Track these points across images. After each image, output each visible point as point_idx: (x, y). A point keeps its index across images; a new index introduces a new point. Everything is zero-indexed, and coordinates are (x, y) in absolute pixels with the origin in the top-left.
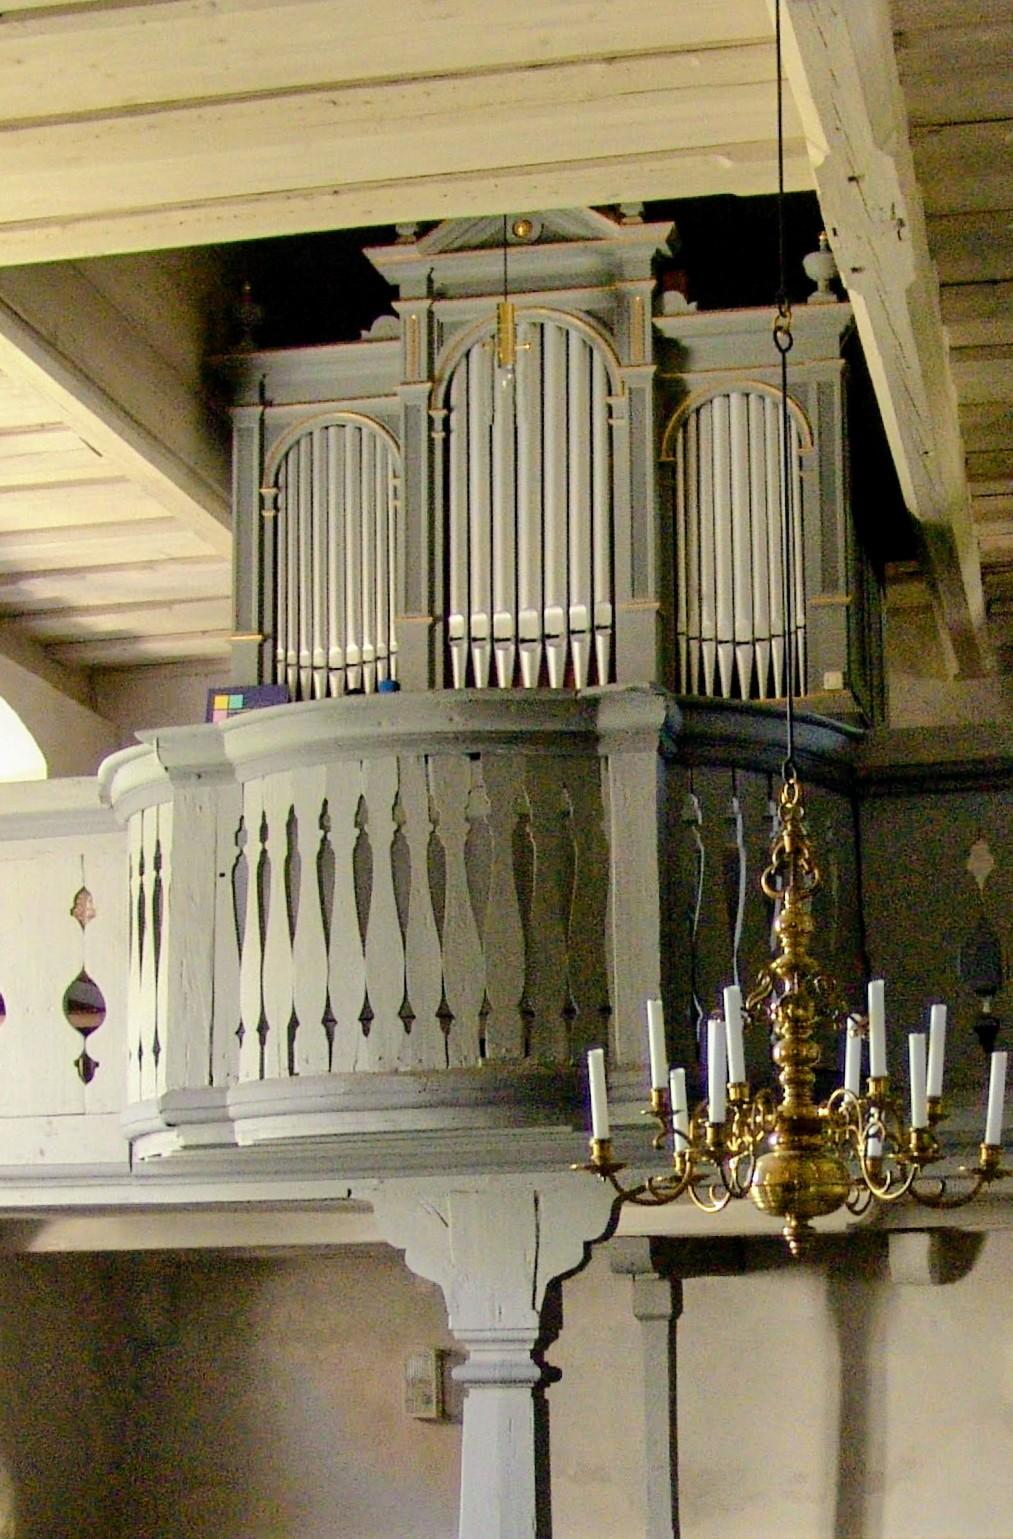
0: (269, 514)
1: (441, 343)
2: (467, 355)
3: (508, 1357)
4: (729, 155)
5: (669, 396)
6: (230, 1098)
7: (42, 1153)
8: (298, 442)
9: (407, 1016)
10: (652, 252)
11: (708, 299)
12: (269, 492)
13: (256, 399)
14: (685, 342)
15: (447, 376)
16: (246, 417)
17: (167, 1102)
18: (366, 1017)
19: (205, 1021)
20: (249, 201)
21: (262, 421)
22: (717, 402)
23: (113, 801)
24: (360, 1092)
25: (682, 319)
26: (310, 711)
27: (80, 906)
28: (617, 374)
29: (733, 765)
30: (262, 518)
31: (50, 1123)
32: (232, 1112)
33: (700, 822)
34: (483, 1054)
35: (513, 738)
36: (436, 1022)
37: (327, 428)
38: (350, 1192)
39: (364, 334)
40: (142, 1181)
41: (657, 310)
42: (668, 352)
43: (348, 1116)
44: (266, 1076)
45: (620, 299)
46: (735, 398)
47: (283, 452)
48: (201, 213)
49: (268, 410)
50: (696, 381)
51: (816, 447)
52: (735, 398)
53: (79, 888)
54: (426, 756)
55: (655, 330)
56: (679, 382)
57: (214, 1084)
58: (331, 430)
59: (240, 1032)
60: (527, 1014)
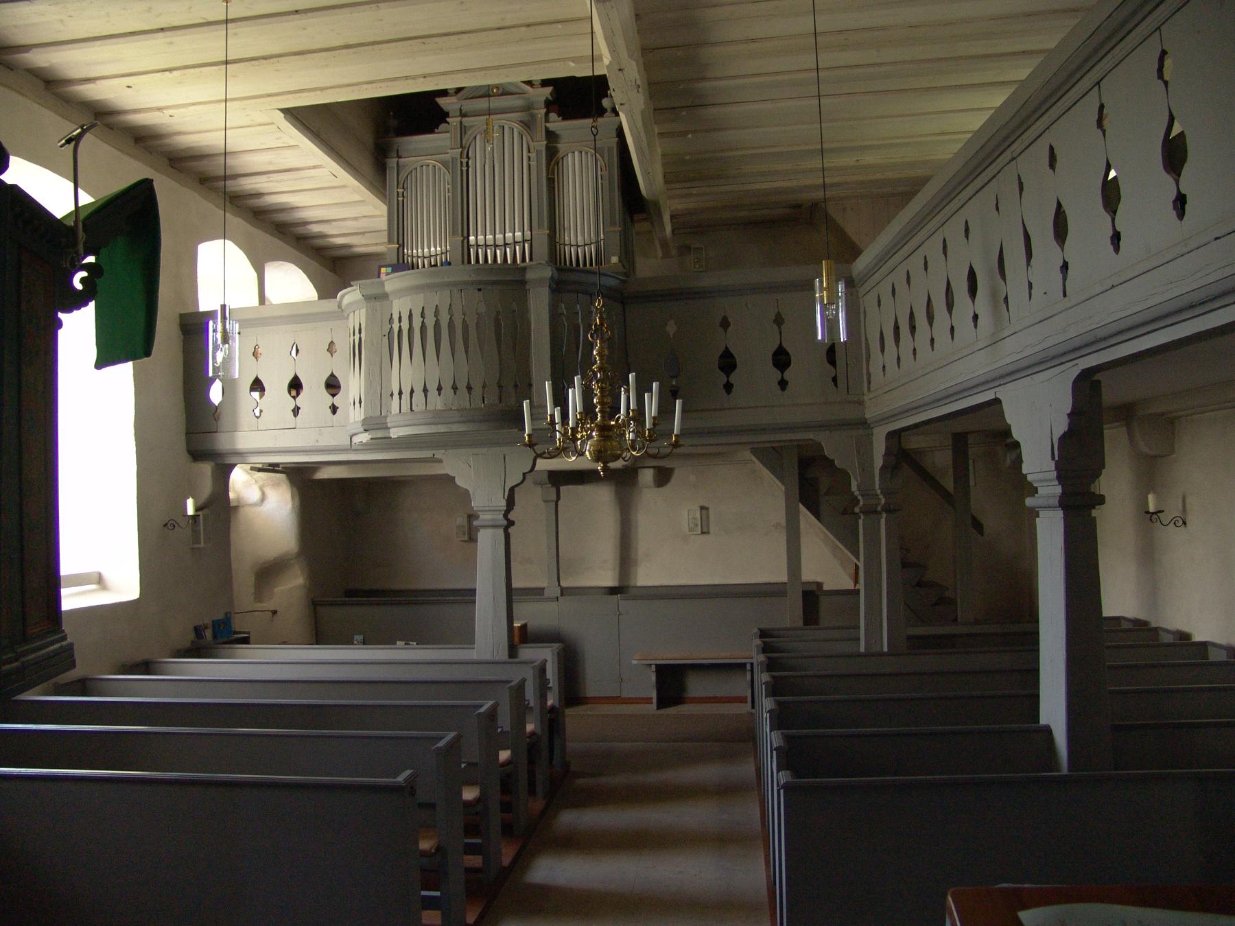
9: (455, 388)
11: (566, 115)
16: (392, 162)
18: (439, 389)
19: (378, 392)
24: (437, 417)
25: (557, 124)
27: (331, 348)
28: (532, 144)
36: (466, 391)
41: (547, 121)
42: (551, 136)
45: (533, 116)
59: (392, 395)
60: (500, 387)
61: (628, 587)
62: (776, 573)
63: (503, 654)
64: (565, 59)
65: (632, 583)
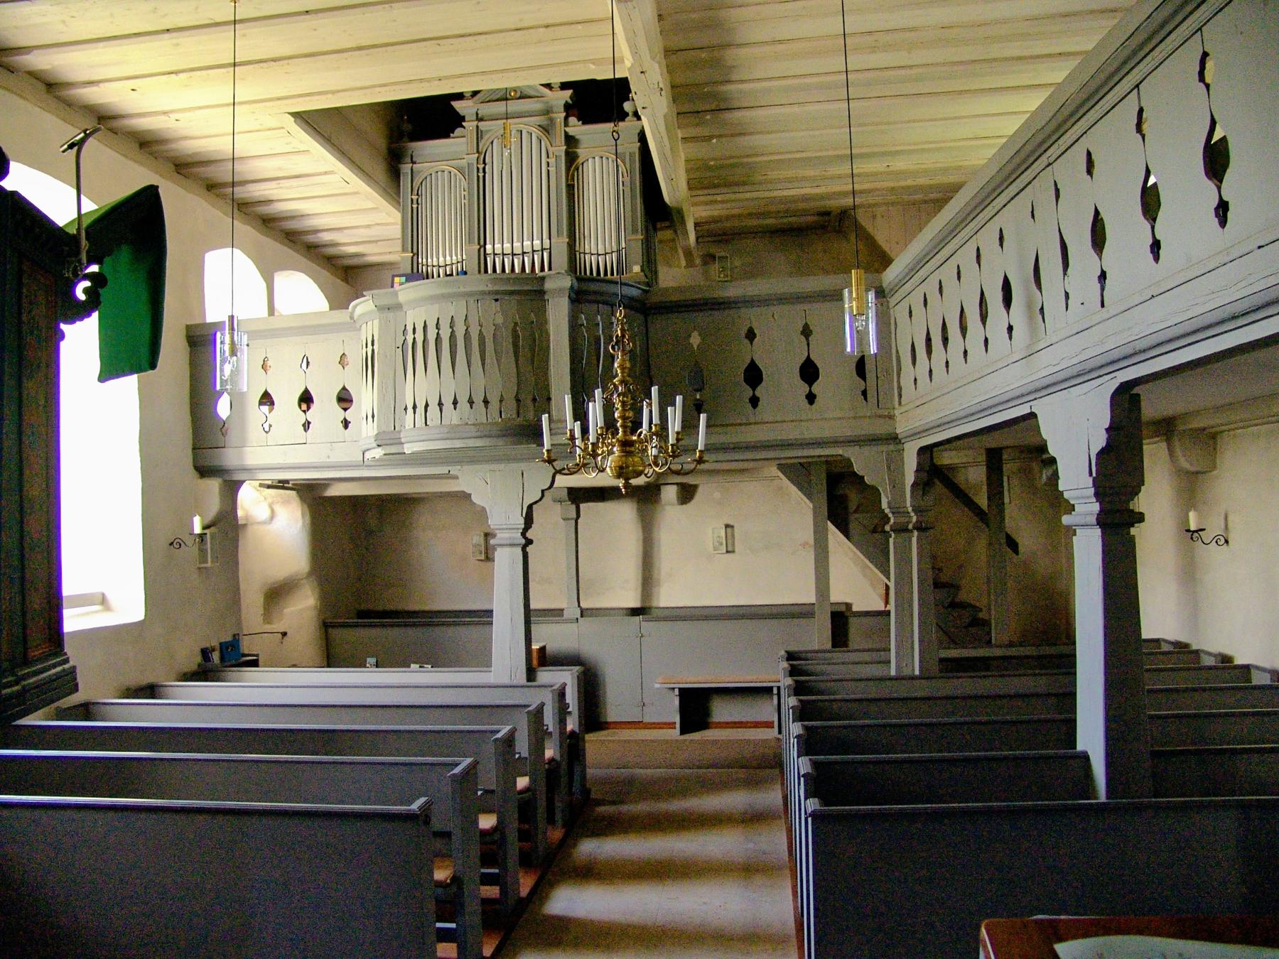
9: (471, 402)
11: (586, 119)
16: (406, 168)
17: (377, 437)
18: (455, 403)
19: (393, 406)
25: (576, 128)
27: (343, 360)
28: (551, 149)
29: (598, 302)
35: (512, 293)
41: (566, 125)
42: (571, 141)
45: (552, 120)
50: (582, 152)
60: (518, 401)
61: (650, 608)
63: (521, 678)
65: (655, 604)
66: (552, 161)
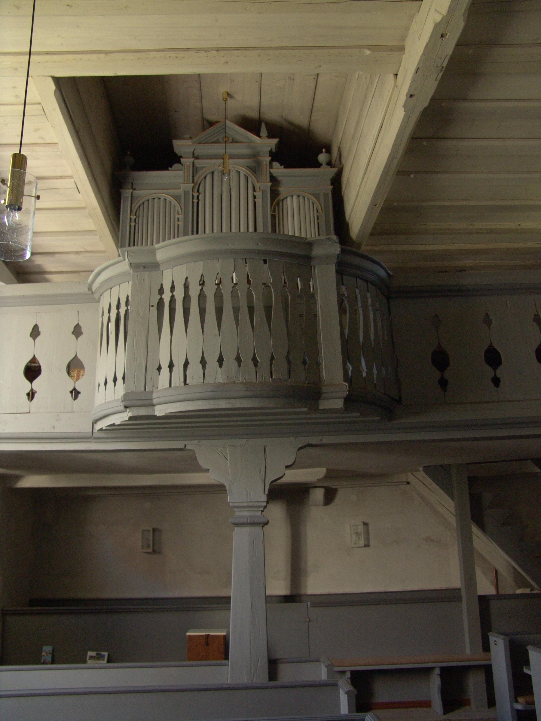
0: (133, 224)
1: (197, 173)
2: (205, 177)
3: (252, 513)
4: (369, 49)
5: (274, 194)
6: (155, 395)
7: (54, 427)
8: (144, 203)
9: (238, 359)
10: (269, 149)
11: (287, 165)
12: (133, 217)
13: (130, 187)
14: (279, 178)
15: (199, 183)
16: (127, 193)
17: (125, 397)
18: (221, 361)
19: (144, 366)
20: (182, 51)
21: (132, 195)
22: (289, 199)
23: (93, 290)
24: (218, 391)
25: (278, 170)
26: (198, 239)
27: (77, 331)
28: (257, 185)
29: (357, 277)
30: (130, 226)
31: (58, 415)
32: (155, 401)
33: (346, 295)
34: (272, 377)
35: (282, 254)
36: (251, 364)
37: (154, 199)
38: (185, 446)
39: (170, 168)
40: (96, 441)
41: (271, 167)
42: (273, 179)
43: (212, 402)
44: (172, 385)
45: (258, 163)
46: (295, 198)
47: (138, 206)
48: (162, 54)
49: (135, 192)
50: (283, 190)
51: (324, 212)
52: (295, 198)
53: (76, 324)
54: (246, 259)
55: (271, 173)
56: (277, 190)
57: (147, 390)
58: (156, 200)
59: (159, 368)
60: (289, 362)
61: (301, 596)
62: (454, 579)
63: (262, 677)
64: (361, 47)
65: (303, 592)
66: (258, 194)
